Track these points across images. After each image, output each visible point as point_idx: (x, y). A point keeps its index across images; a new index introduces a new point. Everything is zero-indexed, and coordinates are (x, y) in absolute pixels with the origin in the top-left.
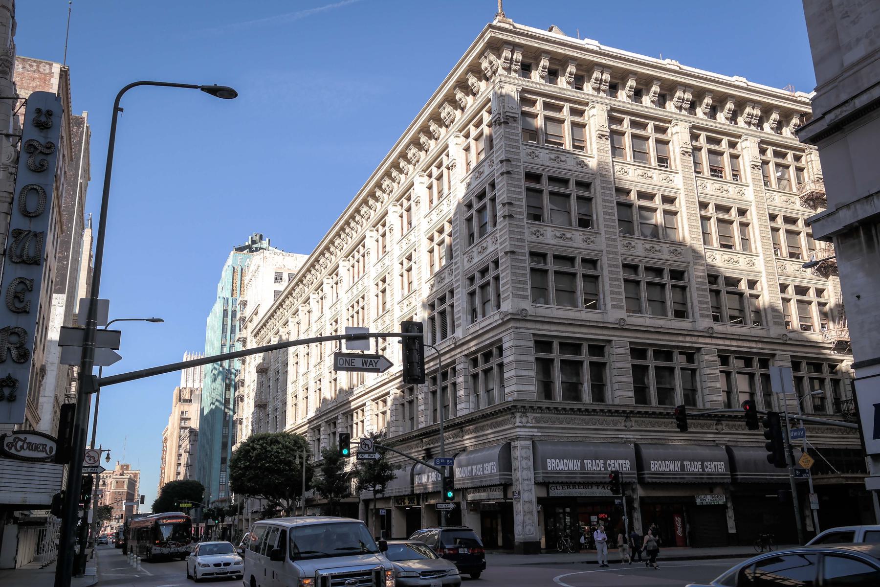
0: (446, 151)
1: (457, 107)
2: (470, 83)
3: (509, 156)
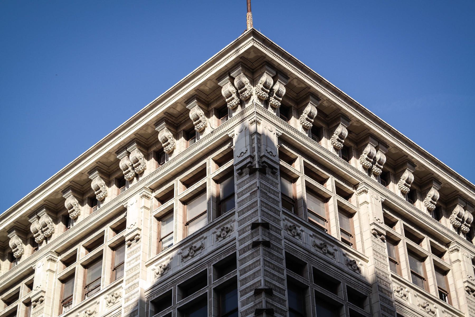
0: (30, 278)
1: (27, 240)
2: (11, 244)
3: (267, 220)
